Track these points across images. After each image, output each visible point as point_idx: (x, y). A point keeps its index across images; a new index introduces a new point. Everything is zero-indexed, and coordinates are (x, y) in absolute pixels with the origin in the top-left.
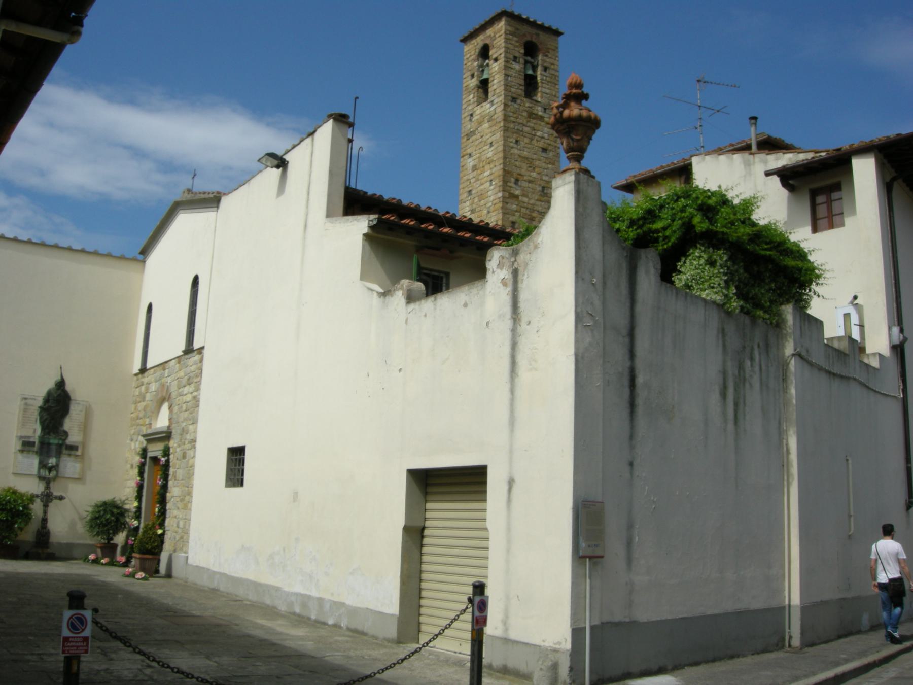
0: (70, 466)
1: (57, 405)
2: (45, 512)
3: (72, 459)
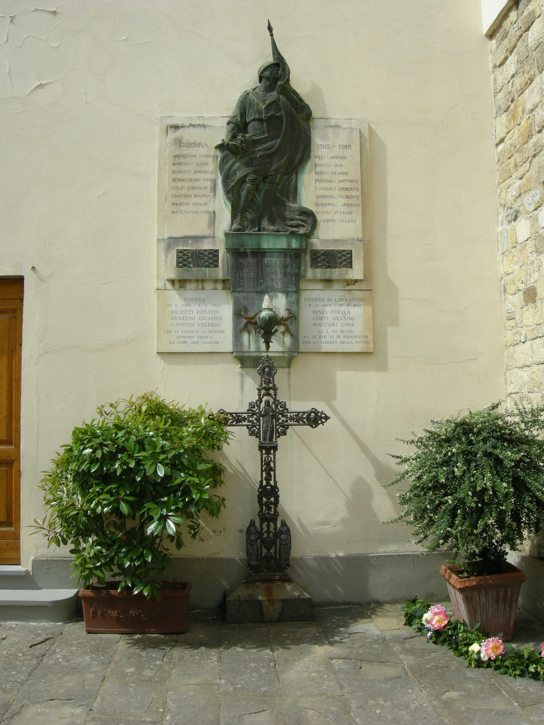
0: (332, 317)
1: (271, 138)
2: (268, 468)
3: (336, 293)
